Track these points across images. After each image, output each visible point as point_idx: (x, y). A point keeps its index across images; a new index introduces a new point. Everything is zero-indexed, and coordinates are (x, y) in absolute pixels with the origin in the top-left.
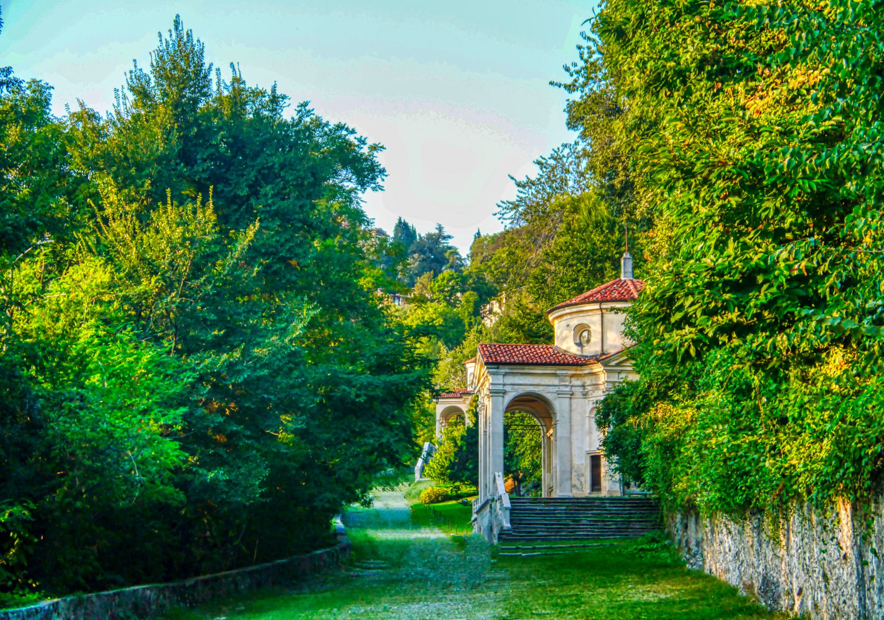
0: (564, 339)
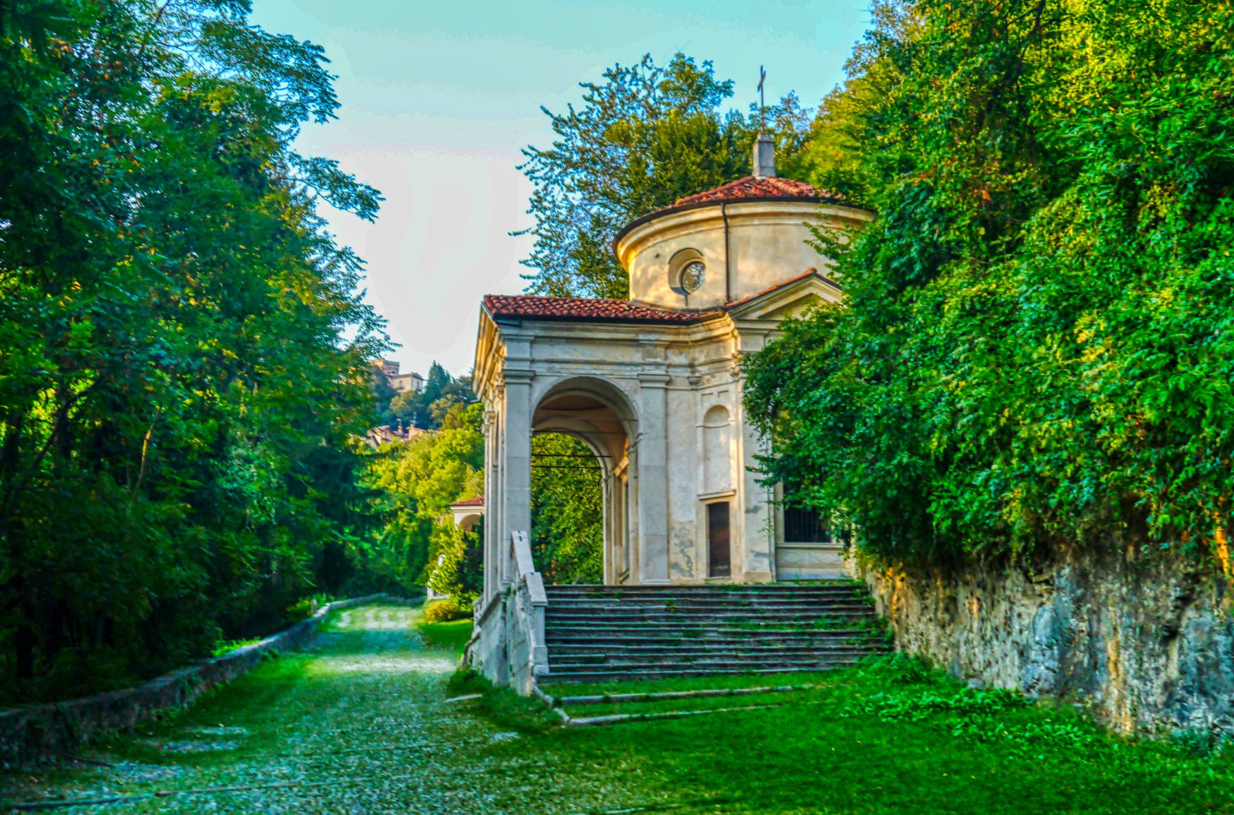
0: (651, 282)
